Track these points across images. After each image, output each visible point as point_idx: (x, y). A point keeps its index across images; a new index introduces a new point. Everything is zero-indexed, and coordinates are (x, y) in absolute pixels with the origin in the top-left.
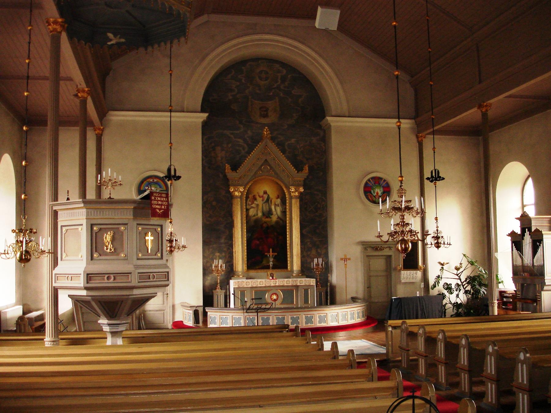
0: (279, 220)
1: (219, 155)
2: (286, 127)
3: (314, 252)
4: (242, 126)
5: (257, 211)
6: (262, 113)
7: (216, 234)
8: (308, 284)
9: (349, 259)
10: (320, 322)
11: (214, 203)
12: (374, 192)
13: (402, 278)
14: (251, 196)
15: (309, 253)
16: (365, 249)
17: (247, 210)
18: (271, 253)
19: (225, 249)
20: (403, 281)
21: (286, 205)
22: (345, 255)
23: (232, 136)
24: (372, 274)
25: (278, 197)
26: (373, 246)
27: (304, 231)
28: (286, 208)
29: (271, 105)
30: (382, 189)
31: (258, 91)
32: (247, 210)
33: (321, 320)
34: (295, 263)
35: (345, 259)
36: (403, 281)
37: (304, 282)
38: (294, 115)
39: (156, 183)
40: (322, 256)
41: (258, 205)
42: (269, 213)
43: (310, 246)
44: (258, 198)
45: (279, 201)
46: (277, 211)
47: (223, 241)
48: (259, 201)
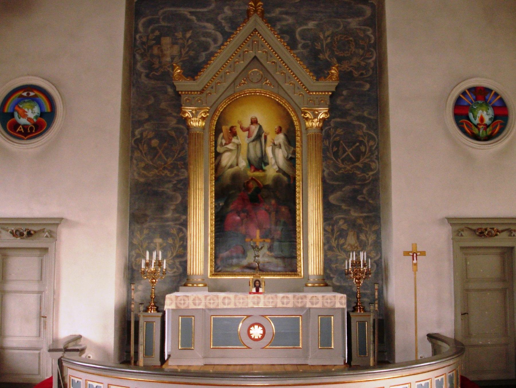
0: (281, 174)
1: (168, 52)
3: (351, 239)
5: (237, 158)
7: (151, 201)
8: (329, 306)
11: (155, 143)
12: (475, 117)
14: (225, 128)
15: (342, 241)
19: (174, 231)
21: (295, 146)
22: (415, 245)
23: (194, 18)
24: (472, 286)
25: (279, 131)
26: (474, 227)
27: (332, 198)
28: (294, 153)
30: (491, 112)
32: (218, 155)
34: (312, 260)
35: (414, 254)
39: (34, 99)
40: (369, 248)
41: (238, 146)
42: (260, 163)
43: (345, 227)
45: (281, 138)
46: (277, 158)
47: (169, 215)
48: (242, 138)
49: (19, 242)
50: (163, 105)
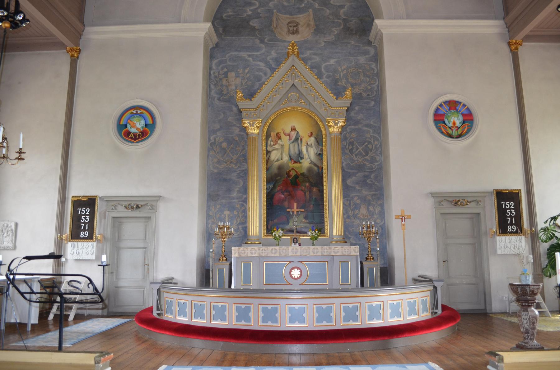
2: (323, 44)
3: (363, 211)
4: (263, 46)
5: (282, 154)
6: (291, 29)
7: (221, 186)
9: (409, 217)
10: (371, 318)
11: (224, 145)
13: (498, 247)
14: (273, 134)
15: (357, 212)
16: (440, 203)
17: (268, 152)
18: (295, 210)
19: (238, 206)
20: (499, 252)
23: (250, 59)
26: (451, 199)
27: (349, 182)
28: (322, 150)
29: (302, 19)
30: (461, 118)
31: (285, 4)
32: (268, 152)
33: (375, 312)
36: (499, 252)
37: (352, 250)
38: (334, 29)
39: (141, 115)
41: (282, 146)
42: (298, 158)
43: (358, 202)
44: (282, 135)
46: (309, 155)
47: (234, 194)
48: (285, 140)
49: (130, 213)
50: (230, 119)
